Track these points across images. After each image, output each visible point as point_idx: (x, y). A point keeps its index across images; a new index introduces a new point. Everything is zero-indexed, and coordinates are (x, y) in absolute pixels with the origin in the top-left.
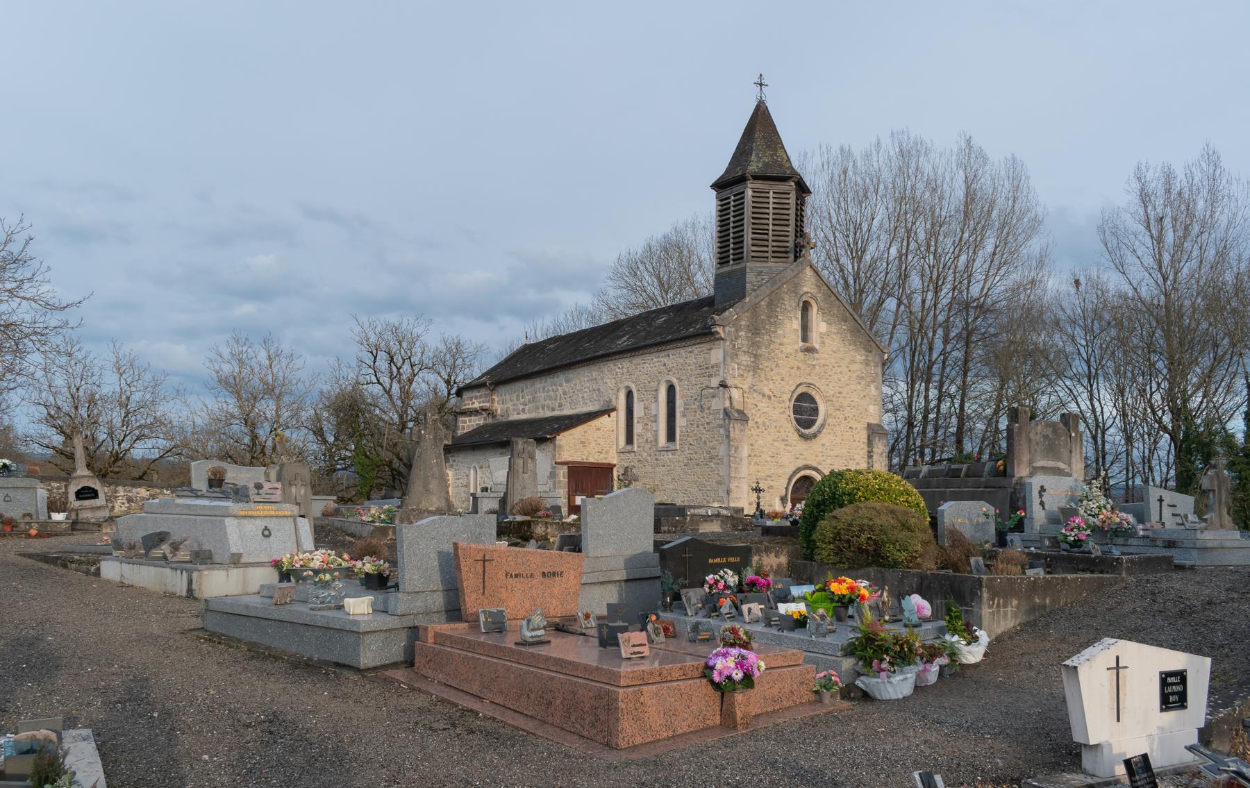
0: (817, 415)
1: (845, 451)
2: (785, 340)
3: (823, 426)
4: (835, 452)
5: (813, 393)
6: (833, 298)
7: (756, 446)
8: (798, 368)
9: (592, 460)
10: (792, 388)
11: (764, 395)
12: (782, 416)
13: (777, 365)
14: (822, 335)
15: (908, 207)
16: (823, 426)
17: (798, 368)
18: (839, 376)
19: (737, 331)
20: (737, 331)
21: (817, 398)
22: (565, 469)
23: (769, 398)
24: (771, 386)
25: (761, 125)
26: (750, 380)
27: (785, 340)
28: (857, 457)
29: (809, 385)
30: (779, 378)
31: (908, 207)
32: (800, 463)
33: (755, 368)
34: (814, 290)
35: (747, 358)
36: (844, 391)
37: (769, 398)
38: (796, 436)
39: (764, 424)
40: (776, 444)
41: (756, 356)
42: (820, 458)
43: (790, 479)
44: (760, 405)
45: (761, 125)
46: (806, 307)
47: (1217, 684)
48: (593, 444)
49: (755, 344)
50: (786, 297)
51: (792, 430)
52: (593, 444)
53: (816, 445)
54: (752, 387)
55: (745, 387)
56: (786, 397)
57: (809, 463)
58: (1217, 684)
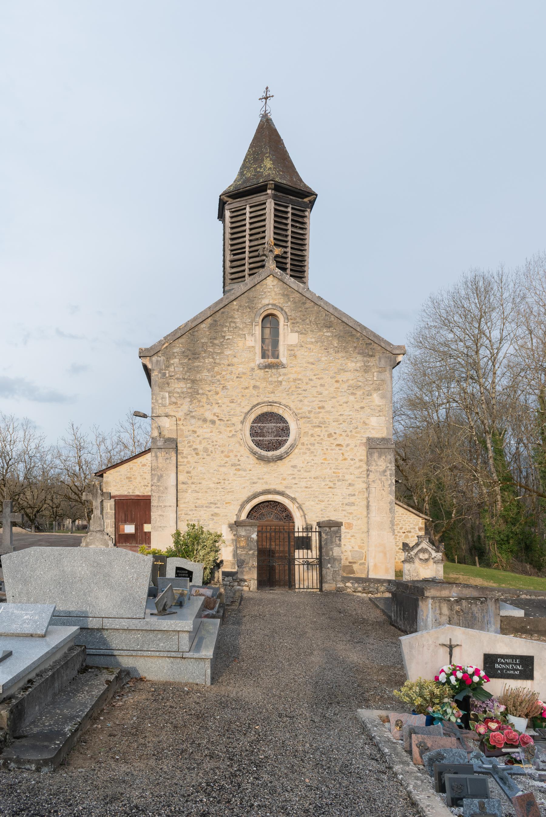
2: (235, 360)
3: (293, 446)
5: (275, 410)
6: (309, 304)
7: (194, 473)
8: (255, 387)
9: (137, 493)
10: (246, 410)
11: (205, 420)
12: (238, 440)
13: (224, 387)
14: (291, 348)
16: (293, 446)
17: (255, 387)
18: (319, 389)
19: (168, 359)
20: (168, 359)
21: (287, 416)
22: (112, 502)
23: (213, 422)
24: (216, 410)
25: (267, 139)
27: (235, 360)
28: (350, 478)
30: (226, 400)
32: (259, 488)
33: (193, 395)
34: (279, 301)
35: (182, 384)
37: (213, 422)
38: (252, 460)
39: (206, 450)
40: (222, 469)
41: (193, 381)
43: (243, 506)
44: (200, 432)
45: (267, 139)
46: (270, 320)
48: (139, 479)
50: (237, 315)
51: (247, 453)
52: (139, 479)
53: (283, 467)
54: (189, 414)
57: (272, 487)
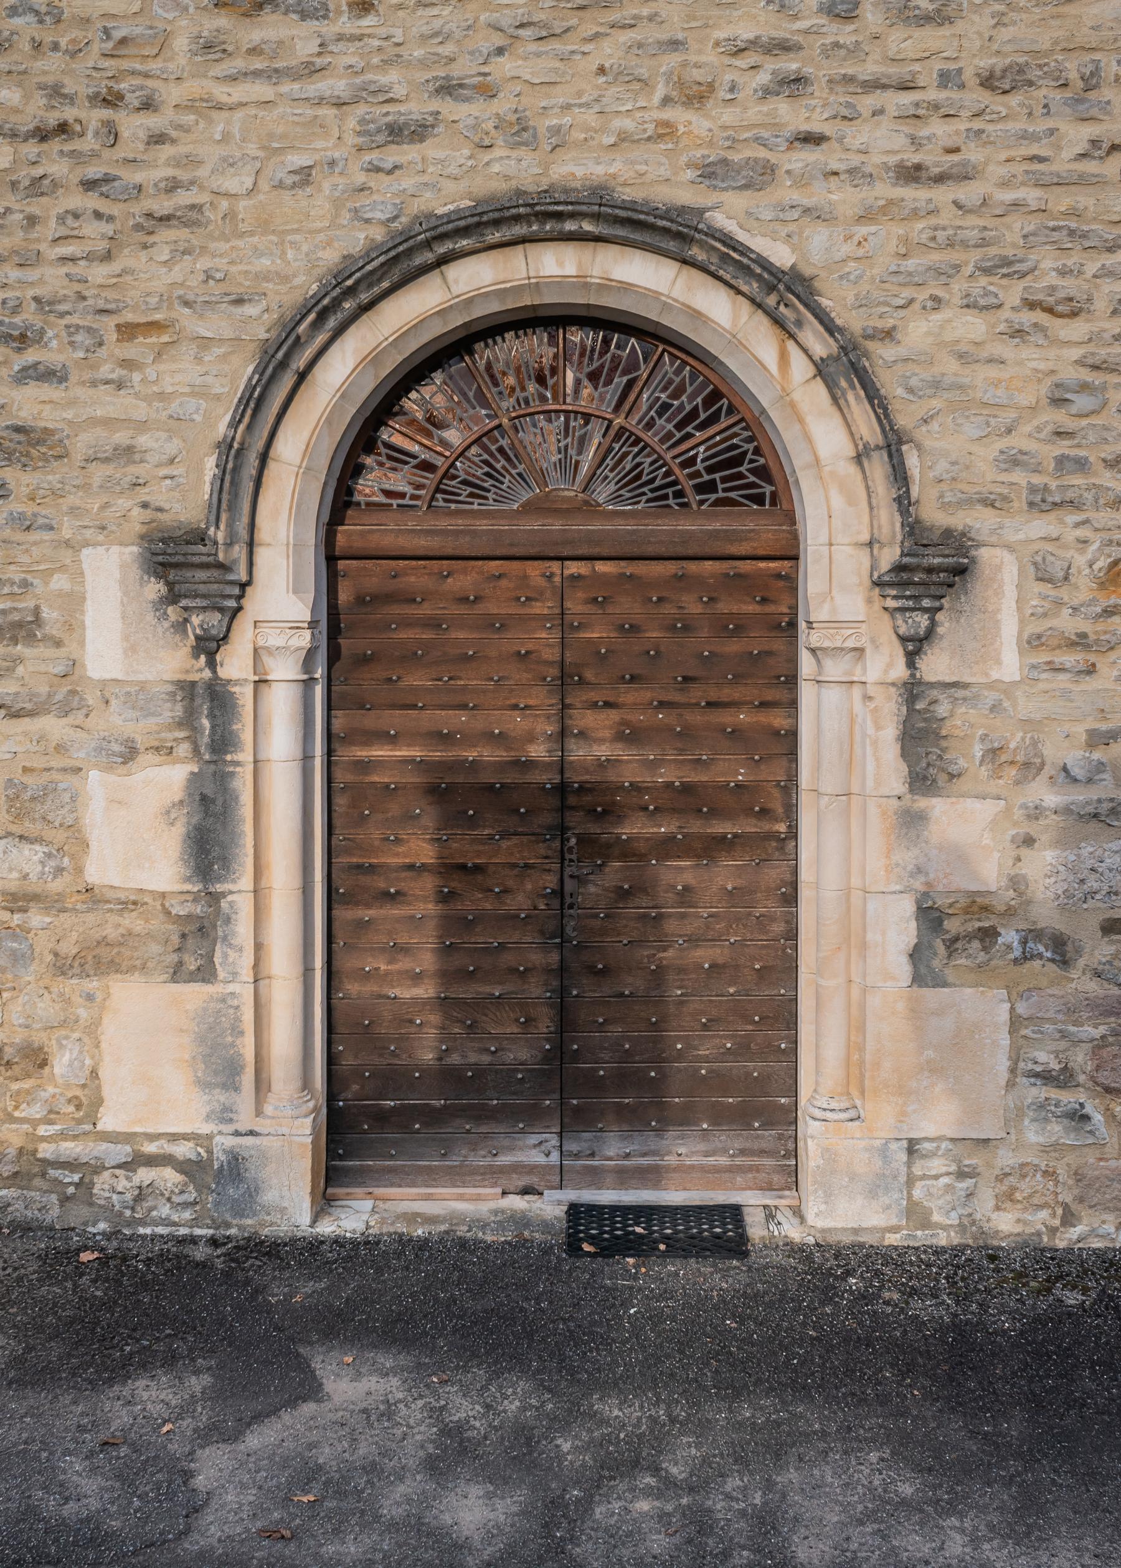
32: (443, 178)
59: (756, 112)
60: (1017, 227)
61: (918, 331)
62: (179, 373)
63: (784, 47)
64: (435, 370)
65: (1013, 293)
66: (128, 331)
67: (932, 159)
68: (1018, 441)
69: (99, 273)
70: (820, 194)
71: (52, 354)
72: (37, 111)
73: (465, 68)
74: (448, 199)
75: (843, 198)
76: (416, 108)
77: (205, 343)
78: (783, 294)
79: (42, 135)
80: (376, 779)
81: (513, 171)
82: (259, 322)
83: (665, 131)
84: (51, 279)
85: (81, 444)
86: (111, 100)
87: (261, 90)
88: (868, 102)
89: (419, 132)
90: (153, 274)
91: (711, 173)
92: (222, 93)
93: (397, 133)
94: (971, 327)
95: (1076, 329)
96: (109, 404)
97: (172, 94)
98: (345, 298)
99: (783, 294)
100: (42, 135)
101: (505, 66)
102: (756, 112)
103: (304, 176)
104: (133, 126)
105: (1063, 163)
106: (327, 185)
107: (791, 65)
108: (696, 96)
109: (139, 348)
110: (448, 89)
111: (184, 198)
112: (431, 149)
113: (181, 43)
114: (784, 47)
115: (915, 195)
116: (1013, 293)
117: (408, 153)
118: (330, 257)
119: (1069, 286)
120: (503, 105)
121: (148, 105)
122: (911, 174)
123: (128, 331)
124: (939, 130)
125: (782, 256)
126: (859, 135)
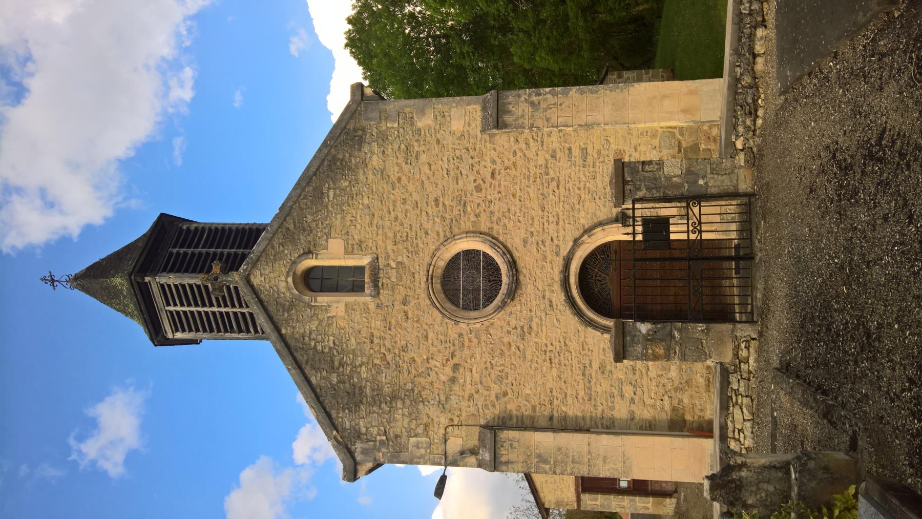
0: (476, 252)
1: (532, 191)
2: (364, 333)
3: (494, 241)
4: (536, 212)
11: (453, 380)
13: (404, 349)
15: (591, 417)
23: (456, 367)
26: (432, 411)
29: (430, 279)
31: (591, 417)
32: (559, 297)
33: (414, 398)
34: (282, 267)
36: (434, 192)
37: (456, 367)
38: (514, 307)
41: (394, 397)
42: (548, 249)
43: (590, 323)
47: (613, 248)
49: (378, 399)
54: (442, 406)
55: (444, 421)
56: (453, 331)
57: (557, 276)
58: (613, 248)
59: (548, 248)
60: (567, 207)
61: (583, 221)
62: (590, 341)
63: (537, 243)
64: (193, 99)
65: (577, 206)
66: (583, 349)
67: (555, 220)
68: (601, 205)
69: (574, 354)
70: (561, 238)
71: (588, 363)
72: (547, 364)
73: (540, 294)
74: (562, 297)
75: (561, 233)
76: (547, 303)
77: (585, 337)
78: (577, 242)
79: (551, 363)
80: (646, 6)
81: (557, 287)
82: (581, 328)
83: (551, 262)
84: (575, 361)
85: (602, 357)
86: (545, 351)
87: (544, 327)
88: (546, 230)
89: (551, 301)
90: (574, 346)
91: (557, 254)
92: (545, 333)
93: (551, 306)
94: (582, 214)
95: (583, 196)
96: (595, 353)
97: (545, 341)
98: (578, 313)
99: (577, 242)
100: (551, 363)
101: (540, 288)
102: (548, 248)
103: (558, 320)
104: (550, 348)
105: (557, 199)
106: (559, 316)
107: (540, 243)
108: (545, 258)
109: (586, 347)
110: (544, 297)
111: (562, 340)
112: (553, 300)
113: (536, 340)
114: (537, 243)
115: (561, 222)
116: (577, 206)
117: (554, 303)
118: (571, 316)
119: (576, 197)
120: (547, 288)
121: (546, 346)
122: (557, 223)
123: (583, 349)
124: (551, 219)
125: (571, 244)
126: (551, 231)
